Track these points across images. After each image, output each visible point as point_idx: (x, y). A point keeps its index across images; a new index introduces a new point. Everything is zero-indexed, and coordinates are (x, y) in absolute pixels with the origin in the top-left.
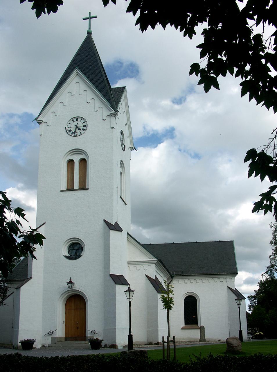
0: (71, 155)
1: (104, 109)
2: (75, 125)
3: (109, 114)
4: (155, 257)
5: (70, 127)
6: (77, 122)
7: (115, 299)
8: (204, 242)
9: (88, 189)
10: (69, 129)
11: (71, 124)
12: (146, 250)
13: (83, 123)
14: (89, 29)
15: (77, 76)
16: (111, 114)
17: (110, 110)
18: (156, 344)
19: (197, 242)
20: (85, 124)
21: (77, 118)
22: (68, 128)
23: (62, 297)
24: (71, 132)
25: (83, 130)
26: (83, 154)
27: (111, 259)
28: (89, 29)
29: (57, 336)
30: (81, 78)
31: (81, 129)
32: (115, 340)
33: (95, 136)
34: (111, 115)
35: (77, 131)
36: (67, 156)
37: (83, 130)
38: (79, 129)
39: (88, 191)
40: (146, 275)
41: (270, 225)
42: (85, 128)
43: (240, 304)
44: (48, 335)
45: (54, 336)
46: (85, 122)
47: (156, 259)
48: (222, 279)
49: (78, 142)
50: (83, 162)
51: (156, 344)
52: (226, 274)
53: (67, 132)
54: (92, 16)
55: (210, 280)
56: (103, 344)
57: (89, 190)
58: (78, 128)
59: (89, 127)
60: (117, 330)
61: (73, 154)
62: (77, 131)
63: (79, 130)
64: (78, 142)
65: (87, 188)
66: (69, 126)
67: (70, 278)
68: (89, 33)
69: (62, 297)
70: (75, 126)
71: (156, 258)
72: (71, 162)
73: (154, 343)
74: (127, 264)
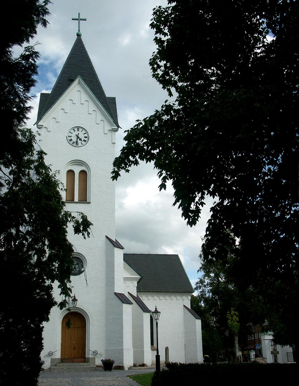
0: (71, 166)
1: (106, 123)
2: (76, 135)
3: (110, 129)
4: (138, 274)
5: (71, 136)
6: (78, 132)
7: (122, 318)
8: (149, 254)
9: (90, 203)
10: (70, 138)
11: (72, 133)
12: (130, 266)
13: (84, 134)
14: (79, 31)
15: (79, 84)
16: (113, 130)
17: (112, 125)
18: (140, 366)
19: (142, 254)
20: (86, 135)
21: (78, 128)
22: (69, 136)
23: (62, 313)
24: (72, 142)
25: (85, 141)
26: (83, 166)
27: (116, 277)
28: (79, 31)
29: (57, 357)
30: (83, 87)
31: (82, 140)
32: (123, 361)
33: (97, 149)
34: (113, 131)
35: (79, 142)
36: (68, 166)
37: (85, 141)
38: (81, 140)
39: (90, 204)
40: (128, 292)
41: (202, 237)
42: (86, 139)
43: (157, 319)
44: (48, 357)
45: (53, 357)
46: (86, 133)
47: (139, 277)
48: (179, 297)
49: (80, 153)
50: (83, 174)
51: (140, 366)
52: (183, 292)
53: (68, 141)
54: (81, 17)
55: (173, 297)
56: (114, 365)
57: (91, 203)
58: (79, 138)
59: (68, 130)
60: (124, 351)
61: (72, 165)
62: (79, 142)
63: (80, 140)
64: (80, 153)
65: (87, 201)
66: (70, 134)
67: (156, 307)
68: (79, 35)
69: (62, 313)
70: (76, 136)
71: (139, 275)
72: (71, 173)
73: (138, 365)
74: (123, 282)
